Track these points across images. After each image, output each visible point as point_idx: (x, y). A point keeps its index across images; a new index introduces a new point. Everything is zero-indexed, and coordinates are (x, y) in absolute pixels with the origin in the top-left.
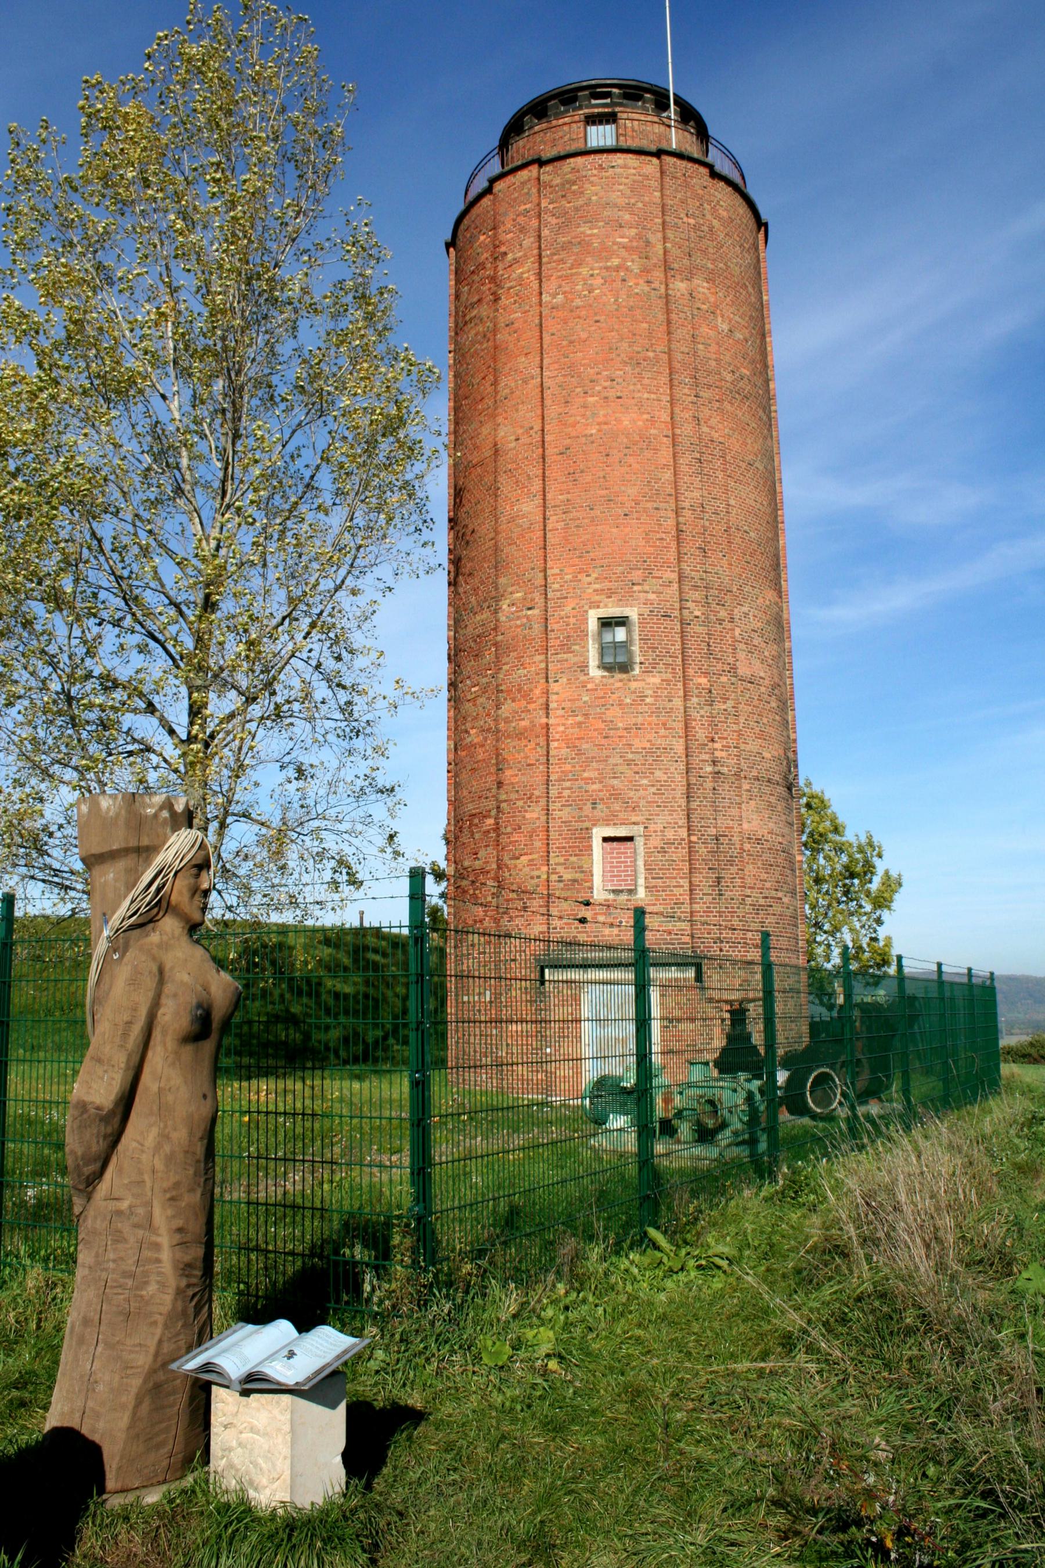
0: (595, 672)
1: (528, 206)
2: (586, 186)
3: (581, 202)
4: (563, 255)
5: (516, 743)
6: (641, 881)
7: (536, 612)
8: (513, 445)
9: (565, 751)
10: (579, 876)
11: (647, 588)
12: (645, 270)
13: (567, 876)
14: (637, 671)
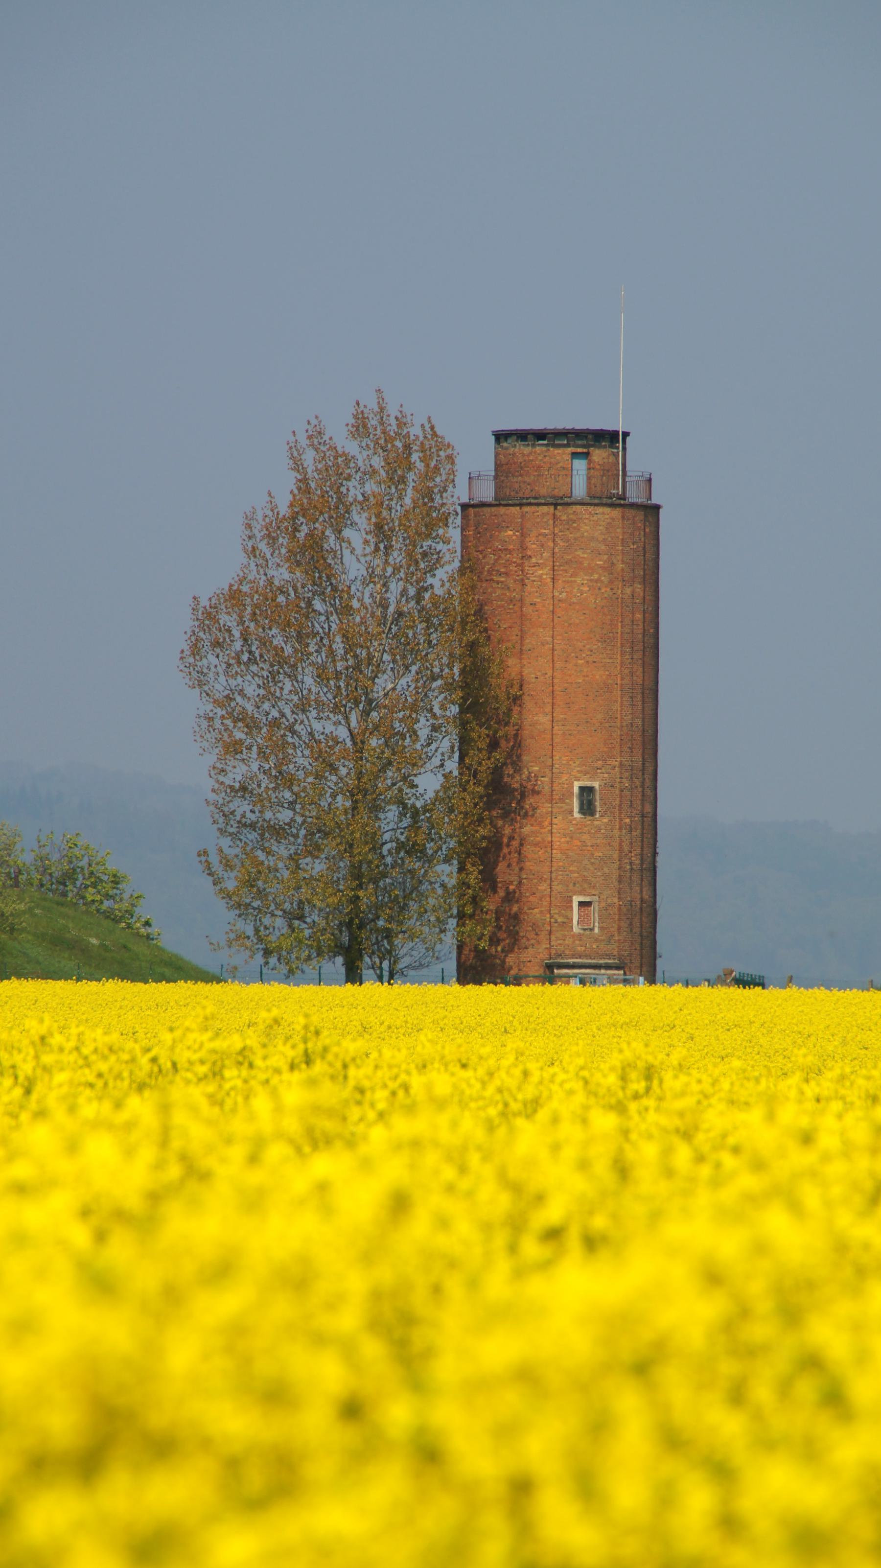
0: (577, 814)
1: (546, 531)
2: (581, 525)
3: (578, 535)
4: (566, 567)
5: (533, 848)
6: (597, 924)
7: (546, 779)
8: (534, 680)
9: (559, 855)
10: (565, 920)
11: (603, 771)
12: (611, 582)
13: (560, 920)
14: (597, 816)
